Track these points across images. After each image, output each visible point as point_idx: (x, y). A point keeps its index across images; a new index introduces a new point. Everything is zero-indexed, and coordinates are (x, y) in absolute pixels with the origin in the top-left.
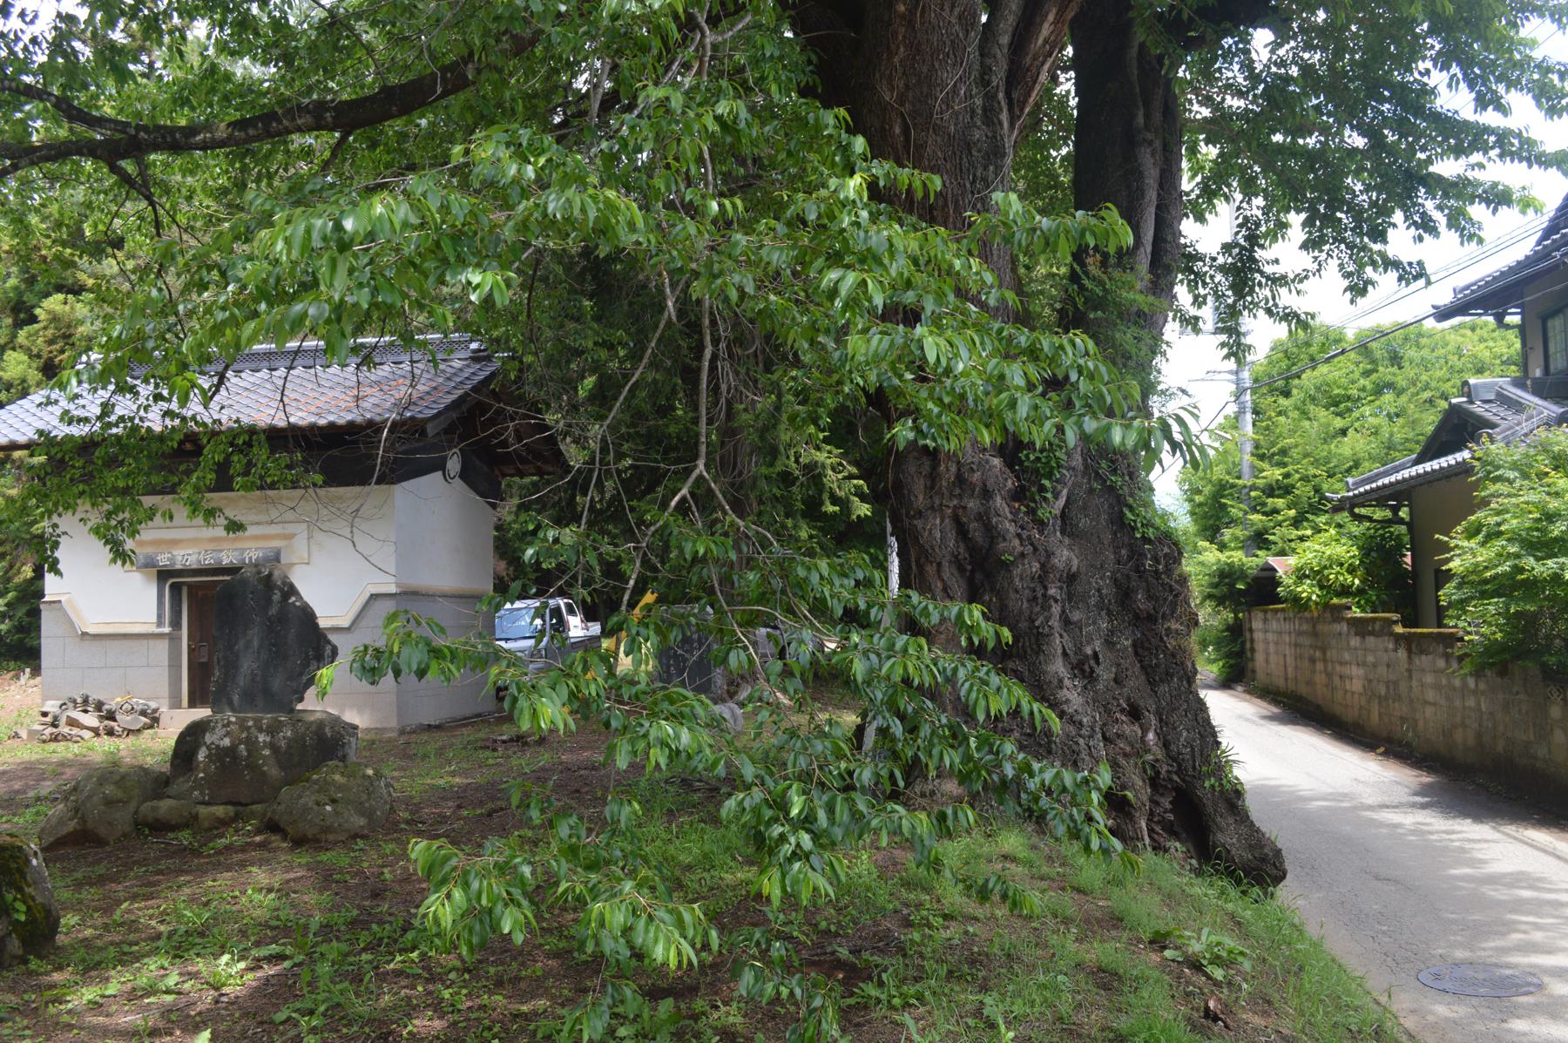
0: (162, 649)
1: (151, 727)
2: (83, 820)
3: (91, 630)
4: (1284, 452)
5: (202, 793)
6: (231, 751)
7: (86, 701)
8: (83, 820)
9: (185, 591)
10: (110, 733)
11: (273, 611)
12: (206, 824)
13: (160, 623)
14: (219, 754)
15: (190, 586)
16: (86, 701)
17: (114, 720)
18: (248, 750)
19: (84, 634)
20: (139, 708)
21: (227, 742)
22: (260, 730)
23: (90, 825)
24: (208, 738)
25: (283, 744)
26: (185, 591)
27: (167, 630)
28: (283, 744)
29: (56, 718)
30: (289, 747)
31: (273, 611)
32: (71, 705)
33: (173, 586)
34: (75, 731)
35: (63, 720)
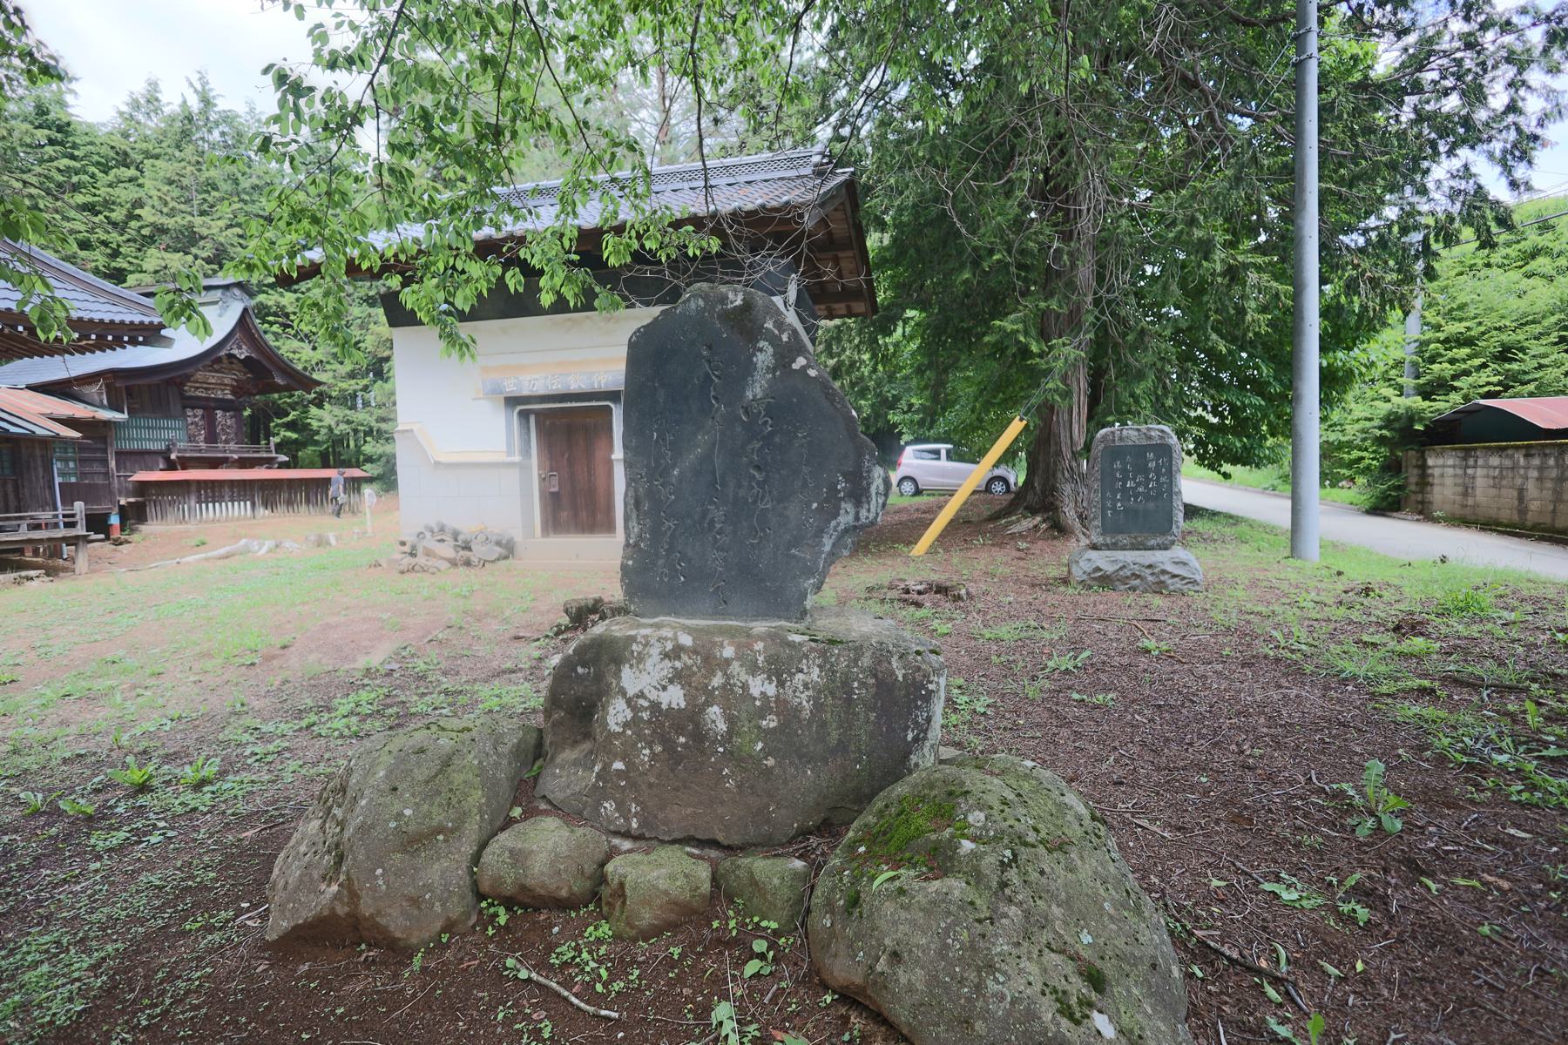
0: (514, 476)
1: (506, 558)
2: (351, 893)
3: (443, 459)
4: (1462, 307)
5: (621, 807)
6: (689, 720)
7: (442, 530)
8: (351, 893)
9: (532, 419)
10: (468, 563)
12: (647, 917)
13: (509, 453)
14: (661, 725)
15: (537, 413)
16: (442, 530)
17: (470, 549)
18: (731, 721)
19: (437, 464)
20: (494, 539)
21: (675, 697)
22: (754, 669)
23: (366, 908)
24: (631, 680)
25: (804, 700)
26: (532, 419)
27: (517, 458)
28: (804, 700)
29: (414, 547)
30: (818, 707)
31: (756, 389)
32: (428, 535)
33: (521, 413)
34: (432, 562)
35: (420, 551)
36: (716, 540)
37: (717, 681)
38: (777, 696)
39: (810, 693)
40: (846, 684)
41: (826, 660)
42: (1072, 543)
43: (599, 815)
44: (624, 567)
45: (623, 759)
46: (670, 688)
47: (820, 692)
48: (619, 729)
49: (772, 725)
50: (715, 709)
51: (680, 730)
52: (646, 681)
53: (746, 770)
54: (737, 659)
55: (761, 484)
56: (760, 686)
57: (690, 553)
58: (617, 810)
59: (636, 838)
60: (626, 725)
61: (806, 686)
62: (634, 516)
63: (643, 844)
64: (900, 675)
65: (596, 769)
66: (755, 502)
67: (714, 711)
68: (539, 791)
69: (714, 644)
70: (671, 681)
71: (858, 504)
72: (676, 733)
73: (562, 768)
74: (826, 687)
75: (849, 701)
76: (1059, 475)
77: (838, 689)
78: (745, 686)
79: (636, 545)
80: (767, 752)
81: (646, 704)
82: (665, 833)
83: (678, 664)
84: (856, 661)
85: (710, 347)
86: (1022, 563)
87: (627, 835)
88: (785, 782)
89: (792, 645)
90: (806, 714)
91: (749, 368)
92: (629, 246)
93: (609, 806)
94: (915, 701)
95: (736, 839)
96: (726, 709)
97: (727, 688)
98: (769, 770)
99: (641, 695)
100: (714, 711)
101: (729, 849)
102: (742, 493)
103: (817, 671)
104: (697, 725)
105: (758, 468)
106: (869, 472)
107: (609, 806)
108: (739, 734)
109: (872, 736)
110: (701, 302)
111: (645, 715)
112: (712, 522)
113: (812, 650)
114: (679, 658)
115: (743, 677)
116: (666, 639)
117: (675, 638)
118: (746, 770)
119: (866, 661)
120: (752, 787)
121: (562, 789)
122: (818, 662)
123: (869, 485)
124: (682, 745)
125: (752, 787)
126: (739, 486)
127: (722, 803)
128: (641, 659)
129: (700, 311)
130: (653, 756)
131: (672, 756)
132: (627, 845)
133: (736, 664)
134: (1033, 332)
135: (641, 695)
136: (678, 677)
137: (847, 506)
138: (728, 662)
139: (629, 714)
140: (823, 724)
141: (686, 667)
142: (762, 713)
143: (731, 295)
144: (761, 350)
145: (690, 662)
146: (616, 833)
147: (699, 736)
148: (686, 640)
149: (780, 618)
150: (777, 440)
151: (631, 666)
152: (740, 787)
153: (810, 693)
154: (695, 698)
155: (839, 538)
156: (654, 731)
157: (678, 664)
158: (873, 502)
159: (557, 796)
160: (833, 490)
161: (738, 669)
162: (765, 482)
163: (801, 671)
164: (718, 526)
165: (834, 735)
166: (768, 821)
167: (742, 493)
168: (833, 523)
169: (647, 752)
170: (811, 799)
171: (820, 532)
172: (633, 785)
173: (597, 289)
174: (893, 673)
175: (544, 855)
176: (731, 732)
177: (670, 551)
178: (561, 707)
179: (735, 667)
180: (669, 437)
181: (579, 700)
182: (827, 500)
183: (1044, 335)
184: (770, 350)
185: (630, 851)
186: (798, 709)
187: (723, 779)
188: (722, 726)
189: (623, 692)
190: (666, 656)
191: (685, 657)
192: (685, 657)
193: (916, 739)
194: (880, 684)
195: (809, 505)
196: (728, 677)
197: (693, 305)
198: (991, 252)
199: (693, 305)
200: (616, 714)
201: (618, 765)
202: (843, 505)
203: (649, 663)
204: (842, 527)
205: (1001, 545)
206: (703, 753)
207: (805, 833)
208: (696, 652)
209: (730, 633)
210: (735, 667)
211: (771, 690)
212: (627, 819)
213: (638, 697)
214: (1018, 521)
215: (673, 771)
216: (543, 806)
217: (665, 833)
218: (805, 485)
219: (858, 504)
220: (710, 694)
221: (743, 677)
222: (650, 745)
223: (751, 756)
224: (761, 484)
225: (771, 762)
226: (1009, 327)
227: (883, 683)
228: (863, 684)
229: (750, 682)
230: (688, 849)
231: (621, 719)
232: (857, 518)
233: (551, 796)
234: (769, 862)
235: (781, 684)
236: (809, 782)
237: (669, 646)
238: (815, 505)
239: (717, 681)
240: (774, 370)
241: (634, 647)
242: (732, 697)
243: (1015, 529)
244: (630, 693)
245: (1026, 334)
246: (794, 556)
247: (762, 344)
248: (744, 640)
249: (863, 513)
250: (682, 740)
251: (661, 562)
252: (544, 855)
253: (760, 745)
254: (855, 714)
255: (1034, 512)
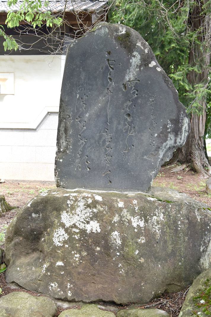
5: (61, 285)
6: (102, 239)
11: (131, 76)
18: (123, 239)
21: (94, 227)
22: (133, 213)
24: (66, 218)
25: (157, 229)
28: (157, 229)
30: (163, 233)
31: (131, 76)
36: (106, 150)
37: (116, 219)
38: (145, 227)
39: (159, 226)
40: (175, 222)
41: (166, 210)
42: (201, 177)
43: (48, 290)
44: (56, 163)
45: (63, 260)
46: (91, 222)
47: (164, 226)
48: (60, 244)
49: (143, 241)
50: (116, 233)
51: (97, 244)
52: (77, 218)
53: (130, 264)
54: (125, 208)
55: (130, 124)
56: (137, 222)
57: (93, 157)
58: (59, 287)
59: (70, 301)
60: (65, 242)
61: (158, 222)
62: (64, 137)
63: (74, 304)
64: (199, 218)
65: (45, 266)
66: (127, 132)
67: (115, 234)
68: (9, 279)
69: (113, 200)
70: (92, 219)
71: (176, 135)
72: (95, 247)
73: (21, 267)
74: (166, 223)
75: (176, 231)
76: (193, 147)
77: (171, 224)
78: (130, 222)
79: (64, 151)
80: (141, 255)
81: (77, 231)
82: (86, 298)
83: (95, 210)
84: (179, 211)
85: (109, 53)
86: (181, 185)
87: (65, 300)
88: (149, 270)
89: (149, 202)
90: (158, 236)
91: (128, 65)
92: (19, 18)
93: (54, 285)
94: (205, 231)
95: (124, 300)
96: (121, 232)
97: (121, 222)
98: (141, 266)
99: (74, 226)
100: (115, 234)
101: (121, 305)
102: (120, 127)
103: (162, 215)
104: (107, 241)
105: (129, 115)
106: (182, 120)
107: (54, 285)
108: (127, 246)
109: (186, 249)
110: (107, 30)
111: (77, 237)
112: (104, 141)
113: (159, 205)
114: (96, 207)
115: (129, 217)
116: (88, 198)
117: (93, 197)
118: (130, 264)
119: (184, 211)
120: (133, 273)
121: (24, 278)
122: (163, 211)
123: (182, 126)
124: (98, 252)
125: (133, 273)
126: (119, 123)
127: (117, 282)
128: (73, 208)
129: (106, 35)
130: (82, 258)
131: (92, 257)
132: (66, 305)
133: (125, 210)
134: (186, 81)
135: (74, 226)
136: (95, 217)
137: (171, 136)
138: (121, 209)
139: (66, 236)
140: (165, 242)
141: (100, 212)
142: (138, 235)
143: (120, 28)
144: (134, 56)
145: (102, 209)
146: (59, 299)
147: (107, 247)
148: (99, 198)
149: (138, 190)
150: (139, 101)
151: (67, 212)
152: (127, 273)
153: (159, 226)
154: (105, 227)
155: (166, 152)
156: (82, 245)
157: (95, 210)
158: (183, 135)
159: (21, 282)
160: (165, 127)
161: (126, 213)
162: (132, 122)
163: (156, 215)
164: (107, 143)
165: (170, 247)
166: (141, 291)
167: (120, 127)
168: (164, 144)
169: (78, 255)
170: (160, 279)
171: (158, 148)
172: (69, 274)
173: (5, 37)
174: (196, 218)
175: (25, 311)
176: (123, 244)
177: (82, 155)
178: (20, 235)
179: (125, 212)
180: (85, 97)
181: (32, 231)
182: (162, 133)
183: (191, 82)
184: (139, 57)
185: (67, 309)
186: (154, 234)
187: (117, 269)
188: (119, 242)
189: (63, 225)
190: (88, 206)
191: (99, 207)
192: (99, 207)
193: (203, 251)
194: (190, 223)
195: (152, 135)
196: (121, 217)
197: (103, 31)
198: (170, 43)
199: (103, 31)
200: (59, 237)
201: (60, 263)
202: (169, 135)
203: (78, 210)
204: (168, 146)
205: (170, 177)
206: (109, 255)
207: (157, 297)
208: (105, 204)
209: (119, 196)
210: (125, 212)
211: (142, 224)
212: (65, 292)
213: (72, 227)
214: (175, 167)
215: (92, 265)
216: (13, 287)
217: (86, 298)
218: (152, 124)
219: (176, 135)
220: (113, 225)
221: (129, 217)
222: (80, 252)
223: (133, 258)
224: (130, 124)
225: (142, 260)
226: (177, 78)
227: (191, 223)
228: (183, 223)
229: (132, 219)
230: (99, 306)
231: (61, 239)
232: (175, 142)
233: (18, 282)
234: (146, 311)
235: (146, 221)
236: (159, 271)
237: (90, 201)
238: (156, 135)
239: (116, 219)
240: (140, 67)
241: (69, 202)
242: (124, 226)
243: (174, 170)
244: (68, 225)
245: (183, 81)
246: (146, 160)
247: (135, 53)
248: (128, 200)
249: (178, 140)
250: (98, 249)
251: (77, 161)
252: (25, 311)
253: (137, 252)
254: (179, 237)
255: (182, 163)
